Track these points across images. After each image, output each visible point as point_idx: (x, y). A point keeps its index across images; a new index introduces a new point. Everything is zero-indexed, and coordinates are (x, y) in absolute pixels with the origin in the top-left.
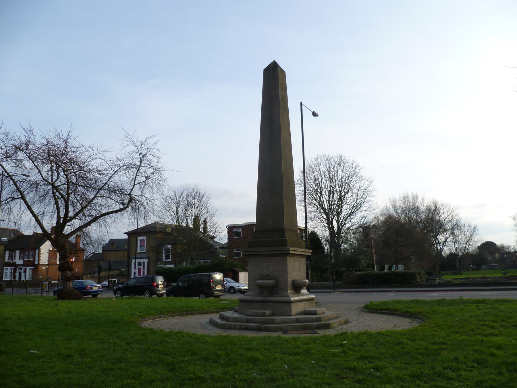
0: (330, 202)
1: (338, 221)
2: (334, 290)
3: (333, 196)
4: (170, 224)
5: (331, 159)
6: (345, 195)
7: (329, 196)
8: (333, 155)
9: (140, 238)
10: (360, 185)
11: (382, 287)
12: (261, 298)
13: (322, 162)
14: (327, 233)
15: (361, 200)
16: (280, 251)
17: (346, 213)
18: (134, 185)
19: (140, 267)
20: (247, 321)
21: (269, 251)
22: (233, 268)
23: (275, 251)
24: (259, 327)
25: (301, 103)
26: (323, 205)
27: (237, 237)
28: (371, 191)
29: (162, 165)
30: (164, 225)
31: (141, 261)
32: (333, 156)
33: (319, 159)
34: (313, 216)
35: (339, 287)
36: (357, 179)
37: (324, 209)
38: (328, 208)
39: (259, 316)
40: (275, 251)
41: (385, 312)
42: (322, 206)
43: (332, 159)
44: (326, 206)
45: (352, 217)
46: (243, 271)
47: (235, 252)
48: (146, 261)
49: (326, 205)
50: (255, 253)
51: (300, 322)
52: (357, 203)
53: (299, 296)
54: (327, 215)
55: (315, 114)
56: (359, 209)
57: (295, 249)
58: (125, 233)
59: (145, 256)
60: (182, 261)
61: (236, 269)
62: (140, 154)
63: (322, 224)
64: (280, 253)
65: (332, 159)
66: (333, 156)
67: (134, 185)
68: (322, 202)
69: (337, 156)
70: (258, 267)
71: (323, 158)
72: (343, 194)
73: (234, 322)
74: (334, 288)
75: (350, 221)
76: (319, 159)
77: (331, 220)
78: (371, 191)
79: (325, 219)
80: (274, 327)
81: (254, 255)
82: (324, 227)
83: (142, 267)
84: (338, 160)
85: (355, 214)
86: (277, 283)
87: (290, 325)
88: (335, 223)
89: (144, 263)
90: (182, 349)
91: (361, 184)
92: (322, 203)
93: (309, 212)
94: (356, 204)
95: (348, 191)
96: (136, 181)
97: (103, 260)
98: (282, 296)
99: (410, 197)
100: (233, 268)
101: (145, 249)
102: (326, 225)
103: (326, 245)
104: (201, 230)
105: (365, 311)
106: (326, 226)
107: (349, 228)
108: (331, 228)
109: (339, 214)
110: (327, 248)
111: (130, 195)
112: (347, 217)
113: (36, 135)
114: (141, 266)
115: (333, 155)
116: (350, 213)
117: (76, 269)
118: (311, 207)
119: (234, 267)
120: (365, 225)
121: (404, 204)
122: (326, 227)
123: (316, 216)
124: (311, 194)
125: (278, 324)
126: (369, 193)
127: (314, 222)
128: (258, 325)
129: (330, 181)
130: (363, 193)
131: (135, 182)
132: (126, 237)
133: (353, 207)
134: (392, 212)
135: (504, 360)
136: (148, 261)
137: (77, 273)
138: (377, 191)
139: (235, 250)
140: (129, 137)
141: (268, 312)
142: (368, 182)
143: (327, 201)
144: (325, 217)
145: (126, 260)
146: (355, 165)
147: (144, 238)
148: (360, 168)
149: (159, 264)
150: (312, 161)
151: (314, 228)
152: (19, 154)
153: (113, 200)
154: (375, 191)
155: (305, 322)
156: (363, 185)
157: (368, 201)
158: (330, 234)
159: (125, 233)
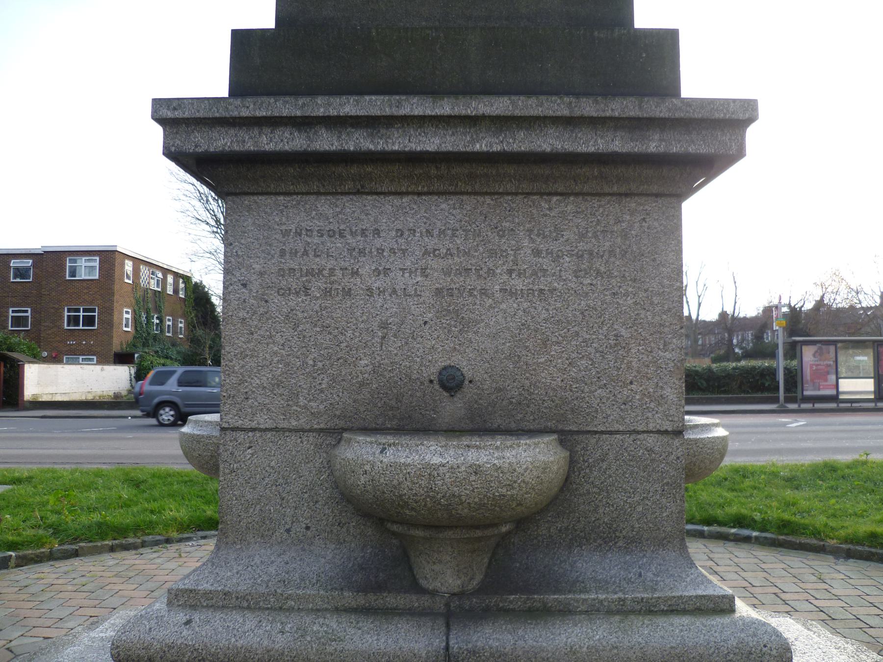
22: (6, 352)
25: (780, 296)
27: (18, 280)
46: (35, 360)
47: (12, 317)
61: (15, 355)
70: (348, 293)
90: (394, 325)
100: (6, 352)
113: (872, 290)
119: (9, 351)
135: (72, 644)
139: (13, 312)
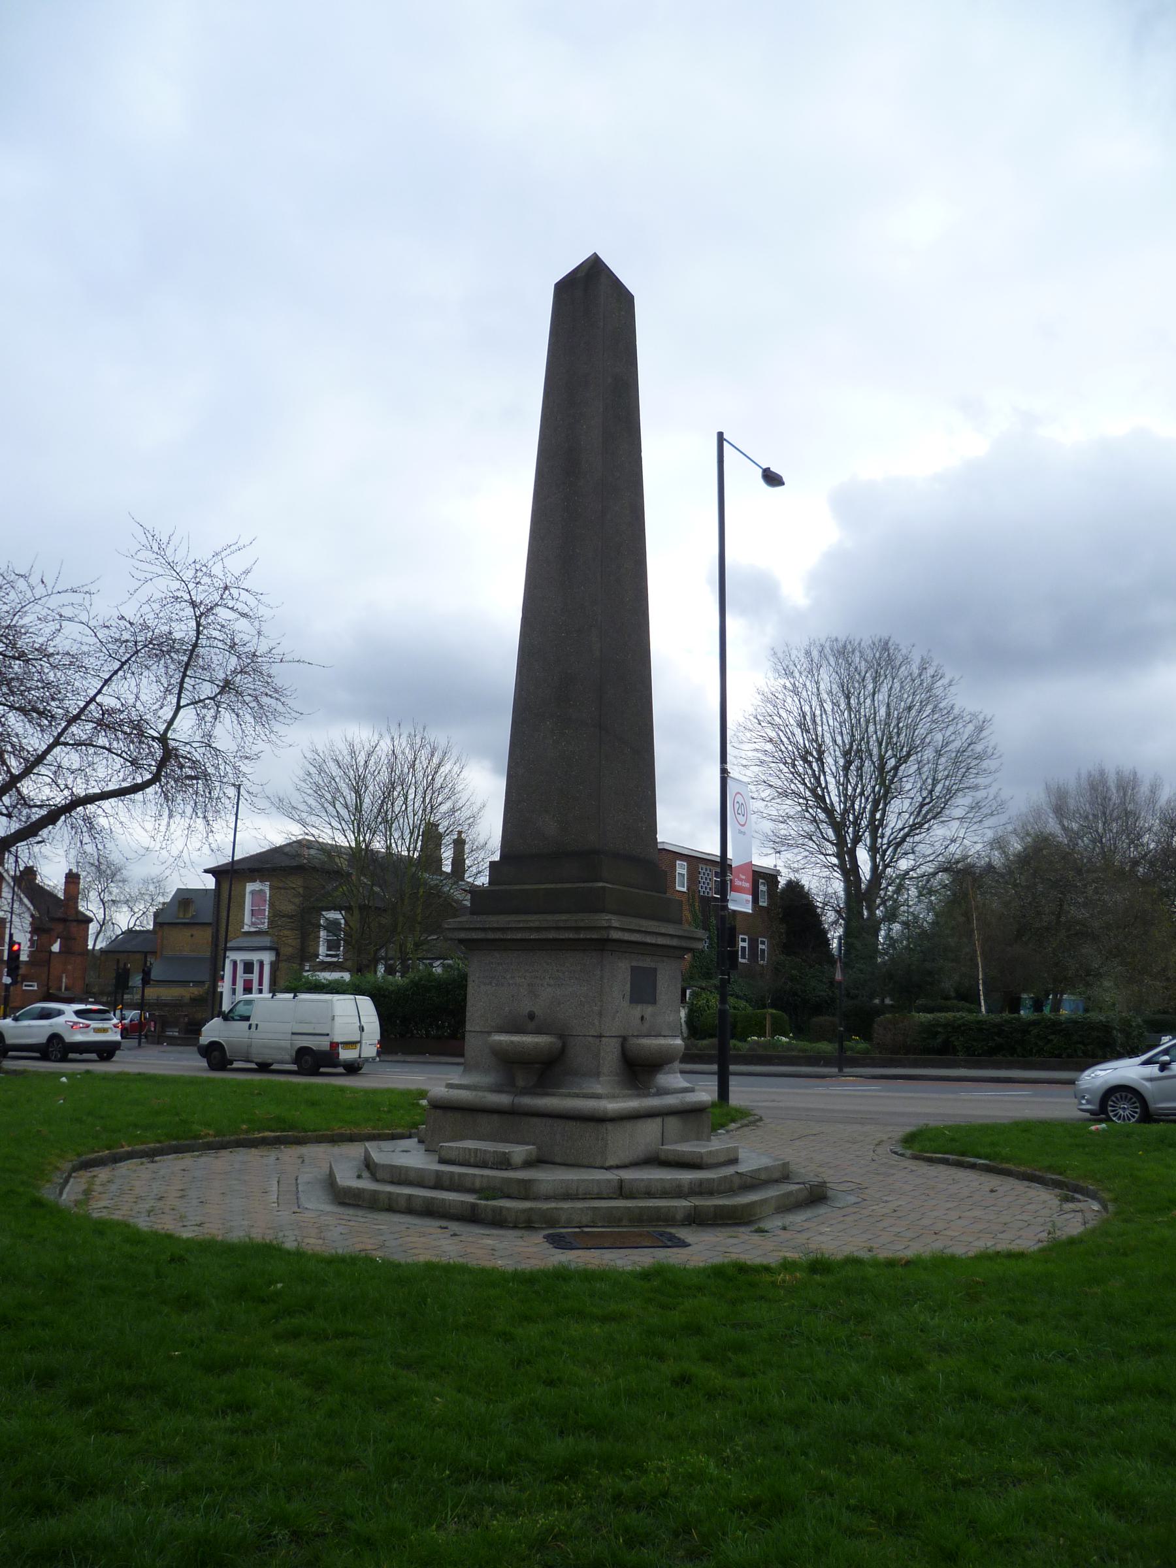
0: (849, 787)
1: (873, 850)
2: (841, 1070)
3: (860, 768)
4: (336, 845)
5: (853, 652)
6: (896, 768)
7: (846, 768)
8: (861, 640)
9: (250, 887)
10: (946, 735)
11: (997, 1066)
12: (503, 1100)
13: (824, 663)
14: (838, 886)
15: (947, 783)
16: (577, 929)
17: (899, 825)
18: (179, 708)
19: (248, 976)
20: (439, 1183)
21: (538, 929)
23: (558, 929)
24: (474, 1206)
25: (720, 436)
26: (827, 798)
28: (980, 757)
29: (272, 644)
30: (317, 845)
31: (255, 957)
32: (860, 644)
33: (815, 654)
34: (792, 832)
35: (854, 1062)
36: (936, 716)
37: (829, 812)
38: (842, 806)
39: (484, 1165)
40: (558, 929)
41: (972, 1160)
42: (823, 798)
43: (857, 654)
44: (833, 797)
45: (917, 838)
48: (267, 957)
49: (835, 799)
50: (491, 936)
51: (631, 1196)
52: (936, 793)
53: (639, 1096)
54: (838, 828)
55: (772, 478)
56: (940, 812)
57: (634, 923)
58: (206, 871)
59: (266, 941)
60: (375, 962)
62: (194, 604)
63: (822, 857)
64: (576, 936)
65: (857, 654)
66: (860, 644)
67: (179, 708)
68: (823, 790)
69: (874, 644)
70: (503, 985)
71: (827, 650)
72: (892, 762)
73: (392, 1183)
74: (843, 1061)
75: (912, 849)
76: (815, 654)
77: (849, 845)
78: (980, 757)
79: (833, 844)
80: (524, 1211)
81: (488, 940)
82: (827, 867)
83: (255, 977)
84: (877, 655)
85: (928, 829)
86: (564, 1042)
87: (588, 1208)
88: (863, 856)
89: (261, 964)
91: (948, 733)
92: (823, 792)
93: (781, 819)
94: (932, 797)
95: (909, 755)
96: (183, 695)
97: (156, 952)
98: (577, 1096)
99: (1112, 783)
101: (266, 921)
102: (835, 861)
103: (836, 922)
104: (447, 868)
105: (902, 1155)
106: (835, 865)
107: (907, 873)
108: (850, 871)
109: (877, 828)
110: (835, 936)
111: (163, 739)
112: (903, 840)
114: (253, 973)
115: (861, 640)
116: (911, 826)
117: (64, 975)
118: (789, 802)
120: (959, 866)
121: (1092, 803)
122: (836, 868)
123: (802, 833)
124: (789, 761)
125: (548, 1198)
126: (975, 762)
127: (796, 851)
128: (470, 1198)
129: (851, 720)
130: (956, 762)
131: (179, 698)
132: (210, 882)
133: (922, 805)
134: (1052, 826)
136: (274, 959)
137: (66, 989)
138: (1000, 757)
140: (155, 548)
141: (519, 1151)
142: (971, 727)
143: (838, 782)
144: (832, 836)
145: (208, 954)
146: (931, 671)
147: (266, 887)
148: (945, 681)
149: (307, 968)
150: (793, 657)
151: (796, 871)
152: (154, 686)
153: (120, 756)
154: (994, 757)
155: (649, 1195)
156: (953, 737)
157: (968, 788)
158: (847, 890)
159: (206, 871)
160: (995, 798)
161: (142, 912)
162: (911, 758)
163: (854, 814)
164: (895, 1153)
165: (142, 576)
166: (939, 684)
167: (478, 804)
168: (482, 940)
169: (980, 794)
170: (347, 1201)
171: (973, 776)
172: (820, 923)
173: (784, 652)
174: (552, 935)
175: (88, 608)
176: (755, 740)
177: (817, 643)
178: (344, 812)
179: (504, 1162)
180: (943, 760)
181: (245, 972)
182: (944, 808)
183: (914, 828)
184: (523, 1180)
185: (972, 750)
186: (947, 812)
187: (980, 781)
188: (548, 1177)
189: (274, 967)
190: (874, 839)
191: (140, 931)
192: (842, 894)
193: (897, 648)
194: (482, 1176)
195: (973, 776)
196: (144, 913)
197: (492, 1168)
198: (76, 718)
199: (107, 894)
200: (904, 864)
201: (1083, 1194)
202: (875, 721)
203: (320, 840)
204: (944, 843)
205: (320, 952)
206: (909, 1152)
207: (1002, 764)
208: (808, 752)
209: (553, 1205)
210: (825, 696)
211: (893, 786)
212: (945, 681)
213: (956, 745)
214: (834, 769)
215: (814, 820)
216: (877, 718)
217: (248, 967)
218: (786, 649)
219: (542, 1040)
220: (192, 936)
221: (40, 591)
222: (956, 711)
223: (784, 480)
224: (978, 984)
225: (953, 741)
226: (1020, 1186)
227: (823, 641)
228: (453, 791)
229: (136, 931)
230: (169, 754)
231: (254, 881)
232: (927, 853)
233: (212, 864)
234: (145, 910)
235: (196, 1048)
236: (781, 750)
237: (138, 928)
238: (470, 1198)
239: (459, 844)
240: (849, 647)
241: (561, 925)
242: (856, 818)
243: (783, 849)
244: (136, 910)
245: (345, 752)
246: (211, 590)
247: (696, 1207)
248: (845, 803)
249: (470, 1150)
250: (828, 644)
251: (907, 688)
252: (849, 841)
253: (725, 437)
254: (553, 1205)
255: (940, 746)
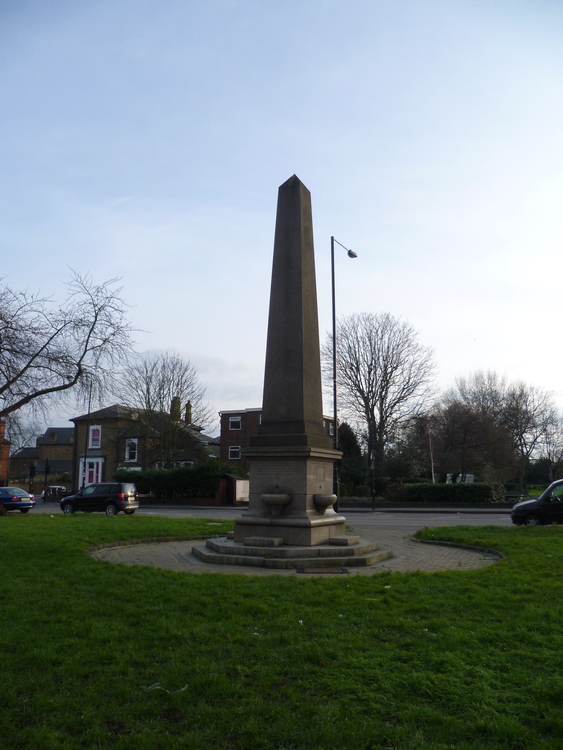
1: (381, 410)
2: (373, 509)
3: (375, 373)
6: (392, 372)
7: (369, 373)
9: (92, 428)
11: (442, 506)
13: (360, 324)
14: (365, 426)
16: (297, 452)
17: (394, 398)
18: (86, 351)
19: (91, 470)
21: (280, 452)
24: (264, 561)
25: (332, 238)
26: (361, 386)
29: (128, 322)
30: (128, 409)
31: (94, 460)
32: (376, 315)
35: (380, 505)
37: (361, 392)
38: (367, 389)
39: (264, 546)
40: (288, 452)
43: (375, 319)
45: (401, 404)
48: (100, 461)
49: (364, 386)
50: (260, 455)
51: (323, 556)
52: (410, 384)
54: (366, 400)
55: (351, 255)
56: (412, 392)
58: (70, 420)
59: (100, 453)
60: (153, 463)
63: (358, 412)
64: (296, 455)
66: (376, 315)
67: (86, 351)
68: (359, 382)
69: (382, 316)
71: (361, 318)
73: (227, 554)
74: (374, 506)
75: (399, 409)
76: (356, 320)
77: (370, 407)
78: (430, 368)
83: (94, 470)
84: (384, 321)
89: (98, 464)
92: (359, 383)
96: (88, 345)
99: (486, 377)
102: (364, 414)
103: (363, 443)
104: (182, 417)
106: (364, 416)
108: (371, 420)
111: (79, 365)
112: (395, 404)
116: (398, 398)
118: (343, 387)
120: (420, 416)
122: (364, 418)
125: (291, 557)
126: (427, 370)
128: (263, 558)
131: (86, 346)
132: (72, 425)
133: (404, 389)
140: (79, 280)
141: (277, 541)
142: (426, 354)
143: (365, 379)
144: (363, 403)
145: (71, 459)
147: (99, 427)
148: (414, 333)
151: (346, 419)
153: (55, 371)
154: (436, 367)
155: (330, 555)
156: (418, 358)
159: (70, 420)
160: (436, 385)
161: (28, 439)
162: (399, 368)
163: (373, 393)
164: (413, 541)
165: (71, 292)
166: (411, 334)
167: (203, 389)
168: (256, 456)
169: (430, 384)
170: (210, 561)
171: (427, 376)
172: (357, 442)
173: (342, 319)
174: (286, 454)
175: (43, 305)
176: (328, 359)
177: (357, 315)
178: (141, 393)
179: (271, 544)
180: (413, 368)
181: (89, 468)
182: (413, 390)
183: (400, 399)
184: (282, 551)
185: (426, 364)
186: (415, 392)
187: (430, 378)
188: (291, 550)
189: (104, 465)
190: (381, 405)
191: (28, 448)
192: (367, 430)
193: (393, 318)
194: (265, 549)
195: (427, 376)
196: (30, 439)
197: (266, 547)
198: (37, 355)
199: (11, 430)
200: (395, 416)
201: (492, 554)
202: (382, 351)
203: (130, 406)
204: (413, 406)
205: (126, 458)
206: (419, 540)
207: (439, 371)
208: (352, 365)
209: (295, 560)
210: (359, 339)
211: (390, 380)
212: (414, 333)
213: (419, 362)
214: (363, 372)
215: (356, 396)
216: (384, 350)
217: (91, 465)
218: (343, 317)
219: (283, 497)
220: (56, 450)
221: (30, 300)
222: (419, 347)
223: (357, 255)
224: (432, 470)
225: (418, 360)
226: (466, 552)
227: (359, 314)
228: (191, 384)
229: (26, 448)
230: (80, 372)
231: (94, 425)
232: (406, 411)
233: (71, 418)
234: (30, 438)
235: (59, 504)
236: (340, 364)
237: (27, 447)
238: (263, 558)
239: (188, 406)
240: (371, 317)
241: (290, 450)
242: (374, 395)
243: (340, 409)
244: (26, 438)
245: (142, 366)
246: (101, 299)
247: (349, 559)
248: (369, 388)
249: (257, 540)
250: (361, 316)
251: (397, 335)
252: (370, 405)
253: (334, 238)
254: (295, 560)
255: (412, 362)
